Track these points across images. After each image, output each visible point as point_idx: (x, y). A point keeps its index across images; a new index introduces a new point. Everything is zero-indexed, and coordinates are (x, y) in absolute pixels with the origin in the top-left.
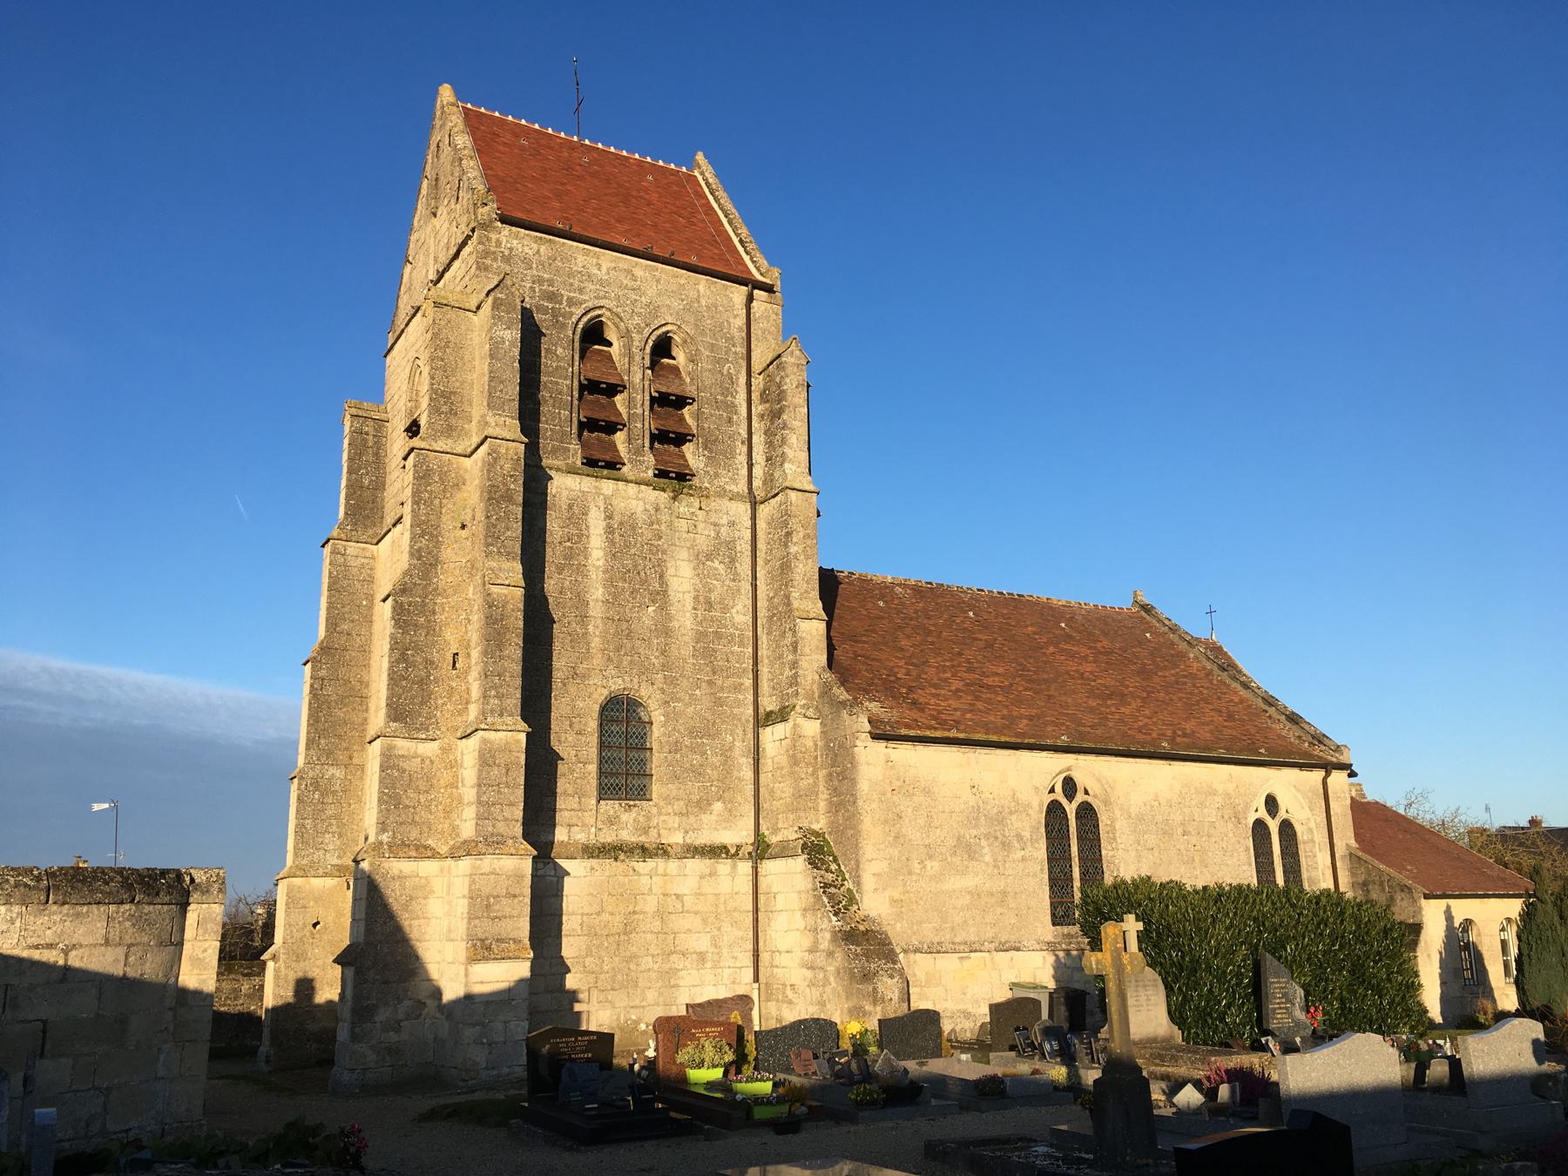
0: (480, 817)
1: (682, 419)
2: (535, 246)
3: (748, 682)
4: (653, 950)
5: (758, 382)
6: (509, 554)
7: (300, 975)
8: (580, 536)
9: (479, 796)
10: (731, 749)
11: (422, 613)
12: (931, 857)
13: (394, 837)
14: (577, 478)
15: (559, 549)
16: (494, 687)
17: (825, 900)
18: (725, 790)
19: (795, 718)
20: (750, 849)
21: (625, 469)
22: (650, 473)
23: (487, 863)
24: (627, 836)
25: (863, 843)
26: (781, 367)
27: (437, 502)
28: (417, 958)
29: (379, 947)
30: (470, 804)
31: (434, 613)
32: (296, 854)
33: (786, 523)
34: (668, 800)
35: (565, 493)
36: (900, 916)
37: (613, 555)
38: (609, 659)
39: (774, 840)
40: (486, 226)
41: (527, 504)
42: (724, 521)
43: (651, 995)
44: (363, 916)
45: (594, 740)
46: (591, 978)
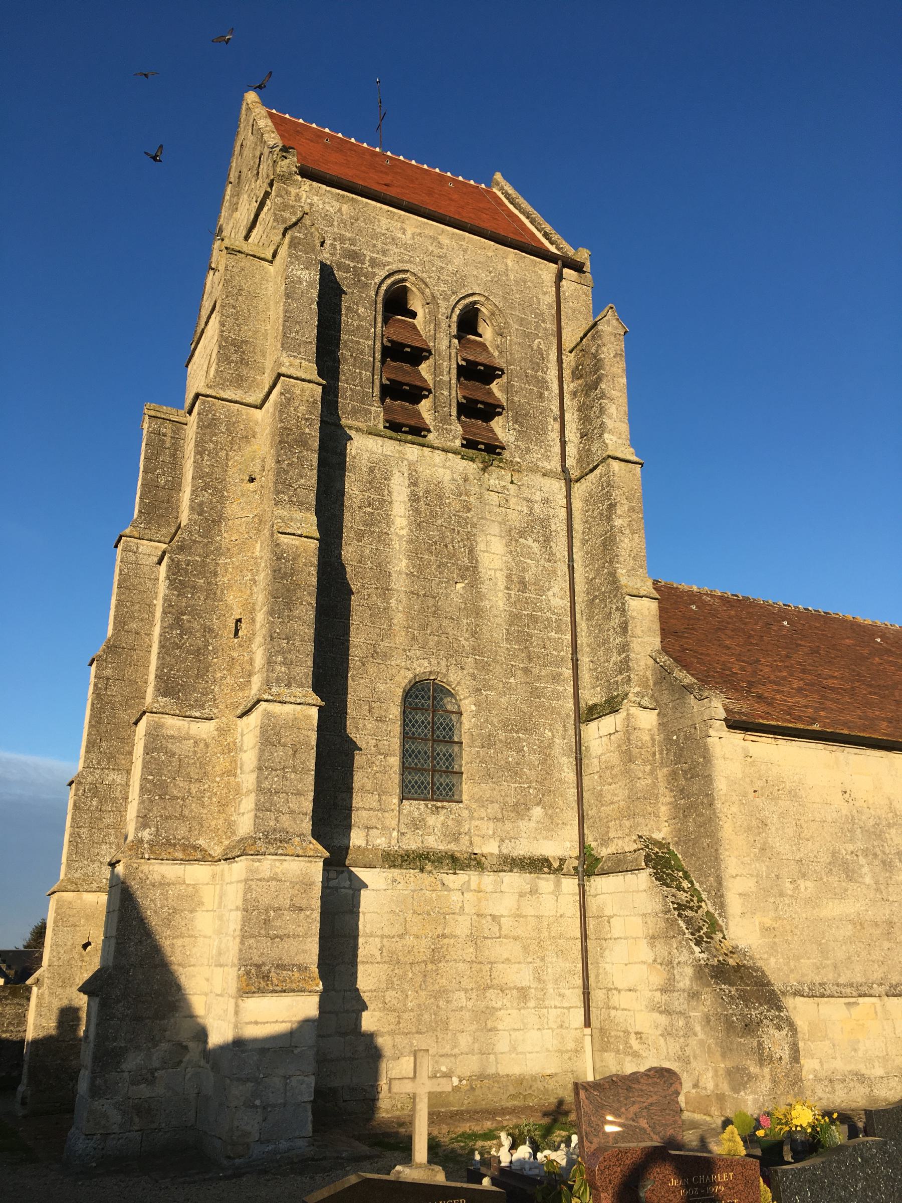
0: (259, 808)
1: (490, 393)
2: (337, 205)
3: (568, 672)
4: (466, 983)
5: (569, 360)
6: (301, 504)
7: (65, 1002)
8: (382, 502)
9: (259, 782)
10: (550, 746)
11: (202, 574)
12: (804, 876)
13: (157, 834)
14: (380, 440)
15: (358, 515)
16: (281, 652)
17: (683, 925)
18: (545, 793)
19: (629, 708)
20: (576, 863)
21: (431, 437)
22: (458, 443)
23: (267, 865)
24: (434, 843)
25: (724, 854)
26: (597, 336)
27: (223, 454)
28: (179, 988)
29: (137, 966)
30: (249, 792)
31: (215, 574)
32: (69, 866)
33: (608, 496)
34: (482, 802)
35: (365, 456)
36: (773, 946)
37: (418, 523)
38: (414, 638)
39: (604, 852)
40: (285, 178)
41: (323, 448)
42: (537, 497)
43: (464, 1041)
44: (114, 933)
45: (397, 729)
46: (392, 1018)
